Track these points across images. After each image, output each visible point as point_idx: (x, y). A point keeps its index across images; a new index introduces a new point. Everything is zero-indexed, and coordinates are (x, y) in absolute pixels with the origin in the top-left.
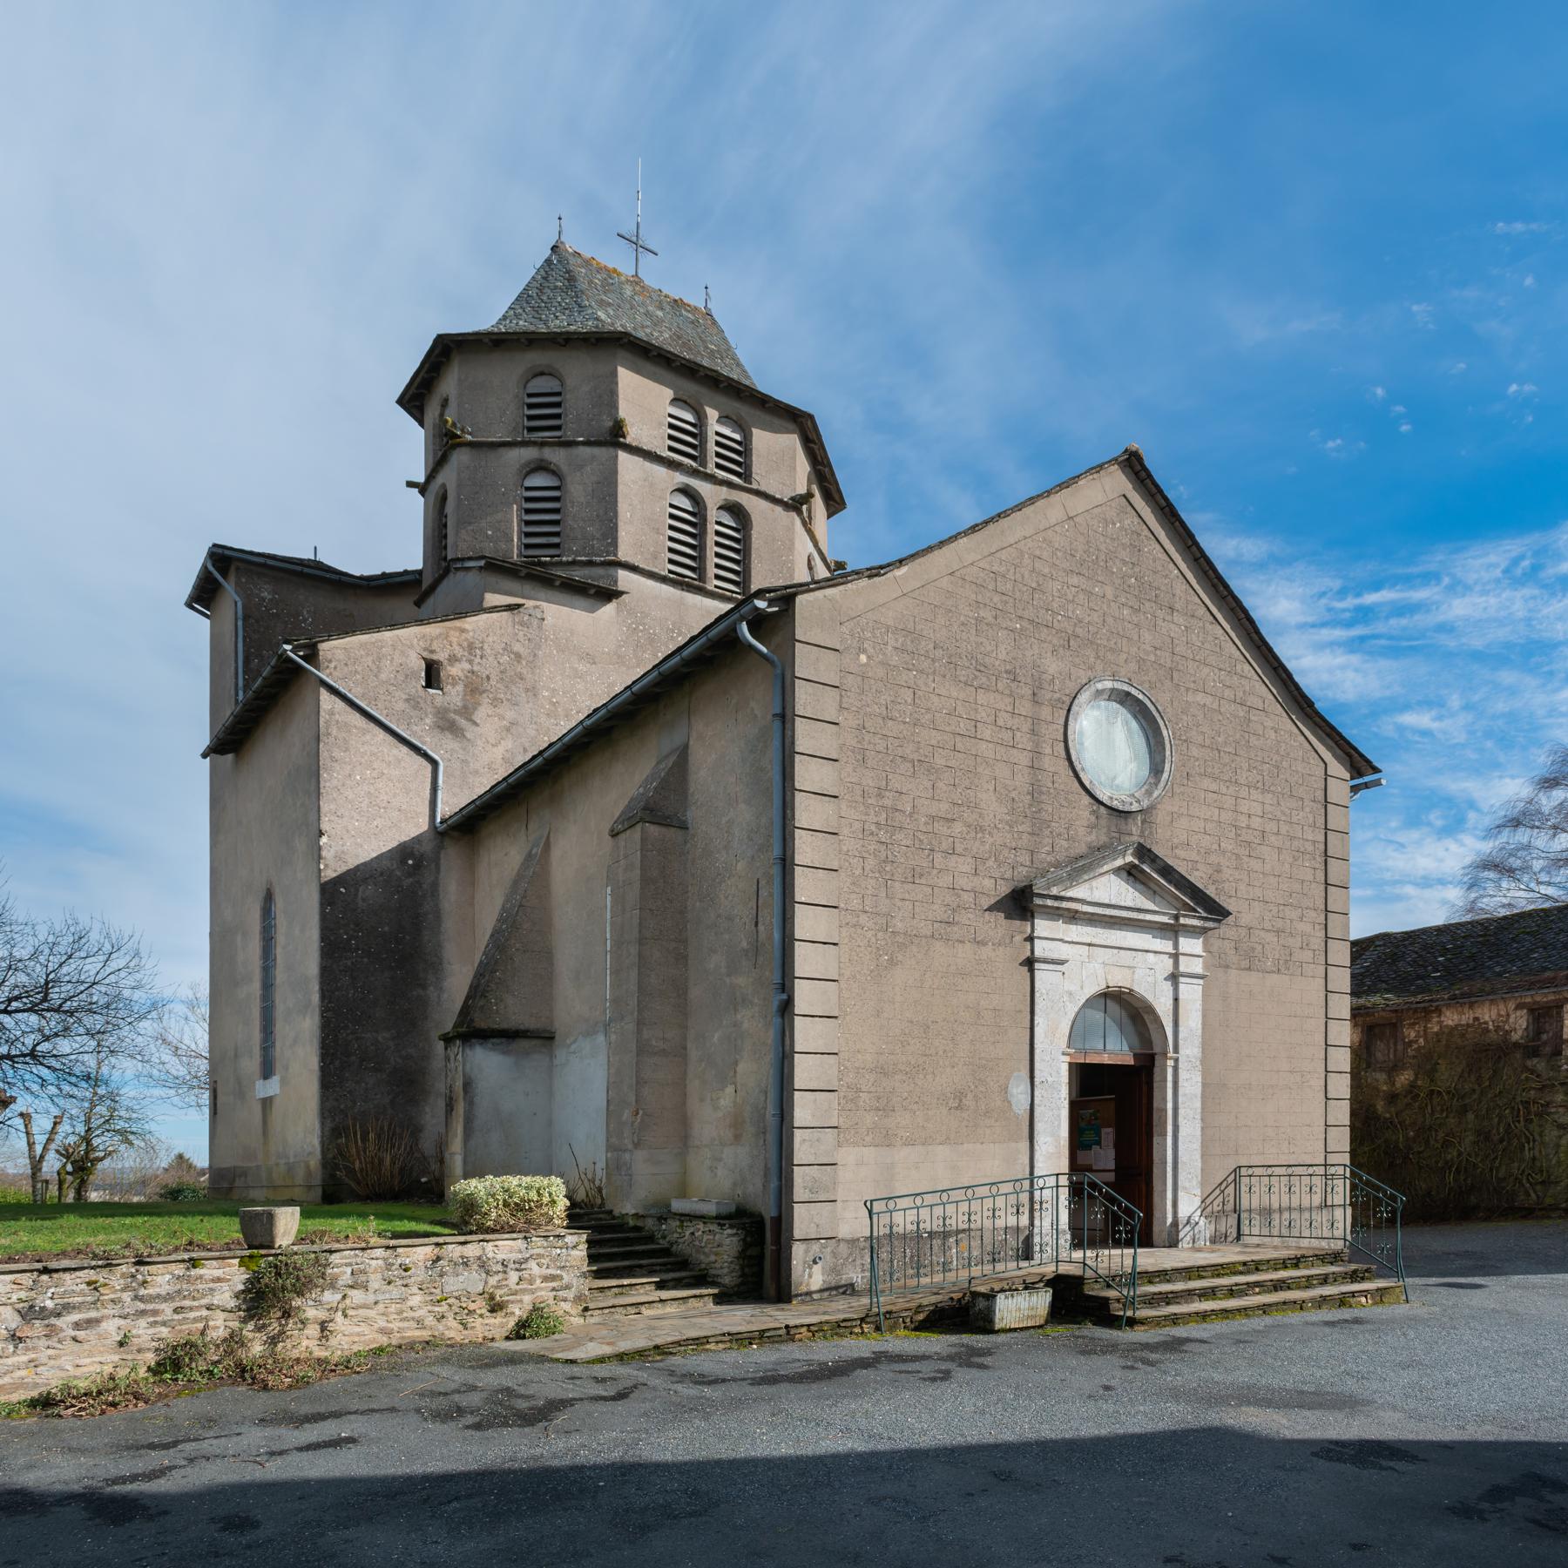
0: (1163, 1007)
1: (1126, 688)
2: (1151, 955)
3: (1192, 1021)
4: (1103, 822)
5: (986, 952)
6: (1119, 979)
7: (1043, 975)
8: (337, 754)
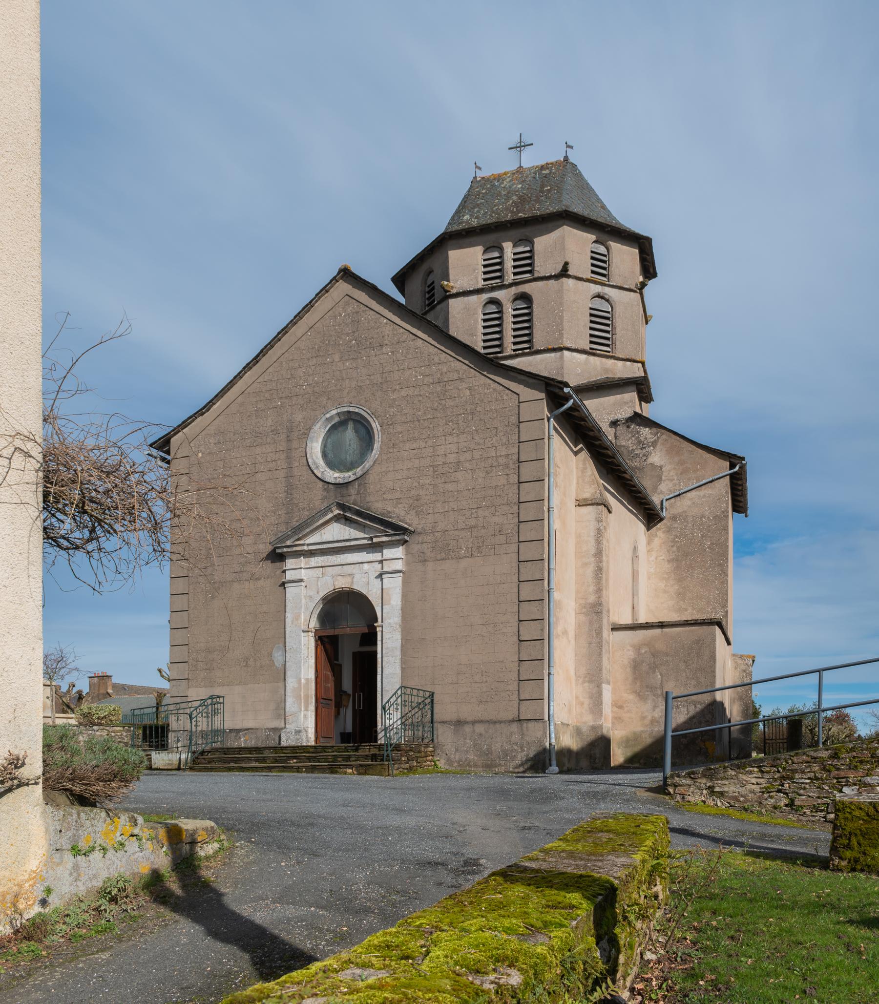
0: (374, 598)
1: (346, 409)
2: (366, 565)
3: (395, 600)
4: (332, 494)
5: (261, 583)
6: (342, 583)
7: (291, 590)
8: (636, 463)
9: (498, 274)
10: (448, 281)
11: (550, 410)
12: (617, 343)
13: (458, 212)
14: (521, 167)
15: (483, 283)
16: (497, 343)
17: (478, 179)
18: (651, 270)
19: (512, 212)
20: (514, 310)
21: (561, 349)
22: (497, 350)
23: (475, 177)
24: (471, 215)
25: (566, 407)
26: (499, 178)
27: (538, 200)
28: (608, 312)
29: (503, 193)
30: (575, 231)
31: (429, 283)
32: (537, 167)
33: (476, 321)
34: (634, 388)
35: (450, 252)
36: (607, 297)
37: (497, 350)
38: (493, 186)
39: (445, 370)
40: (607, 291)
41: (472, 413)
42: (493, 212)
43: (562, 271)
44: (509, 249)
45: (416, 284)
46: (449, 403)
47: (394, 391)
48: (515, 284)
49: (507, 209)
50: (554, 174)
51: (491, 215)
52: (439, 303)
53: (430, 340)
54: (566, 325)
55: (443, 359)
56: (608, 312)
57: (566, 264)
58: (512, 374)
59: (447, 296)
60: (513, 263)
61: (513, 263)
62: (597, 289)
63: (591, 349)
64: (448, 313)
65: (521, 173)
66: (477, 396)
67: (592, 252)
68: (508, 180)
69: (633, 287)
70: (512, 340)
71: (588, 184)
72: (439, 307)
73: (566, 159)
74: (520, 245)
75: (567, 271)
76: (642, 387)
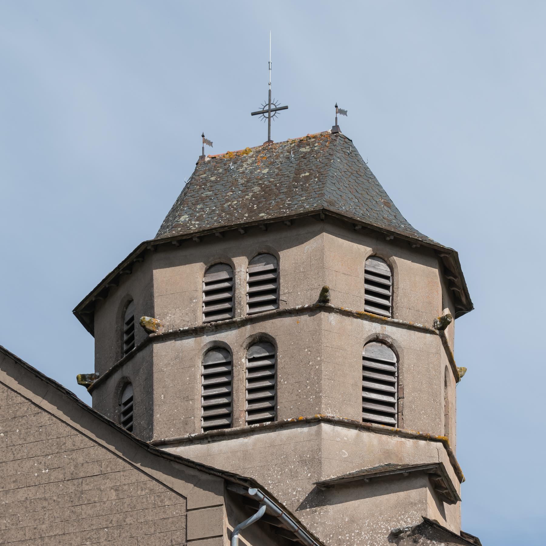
9: (227, 305)
10: (153, 316)
11: (234, 520)
12: (405, 412)
13: (175, 211)
14: (270, 141)
15: (204, 319)
16: (224, 411)
17: (207, 159)
18: (464, 299)
19: (251, 211)
20: (250, 360)
21: (317, 421)
22: (224, 421)
23: (202, 157)
24: (191, 215)
25: (256, 516)
26: (237, 158)
27: (290, 193)
28: (392, 364)
29: (241, 181)
30: (340, 241)
31: (127, 318)
32: (293, 141)
33: (193, 378)
34: (426, 480)
35: (154, 271)
36: (389, 341)
37: (224, 421)
38: (227, 170)
39: (81, 460)
40: (390, 331)
41: (120, 526)
42: (223, 211)
43: (319, 301)
44: (242, 267)
45: (109, 318)
46: (88, 511)
47: (7, 492)
48: (251, 320)
49: (244, 206)
50: (317, 152)
51: (219, 215)
52: (140, 349)
53: (60, 414)
54: (325, 384)
55: (78, 444)
56: (392, 364)
57: (325, 290)
58: (177, 466)
59: (152, 339)
60: (248, 289)
61: (248, 289)
62: (375, 328)
63: (365, 420)
64: (151, 365)
65: (270, 150)
66: (127, 501)
67: (367, 272)
68: (250, 161)
69: (430, 327)
70: (247, 406)
71: (367, 168)
72: (140, 355)
73: (336, 130)
74: (259, 262)
75: (327, 301)
76: (439, 482)
